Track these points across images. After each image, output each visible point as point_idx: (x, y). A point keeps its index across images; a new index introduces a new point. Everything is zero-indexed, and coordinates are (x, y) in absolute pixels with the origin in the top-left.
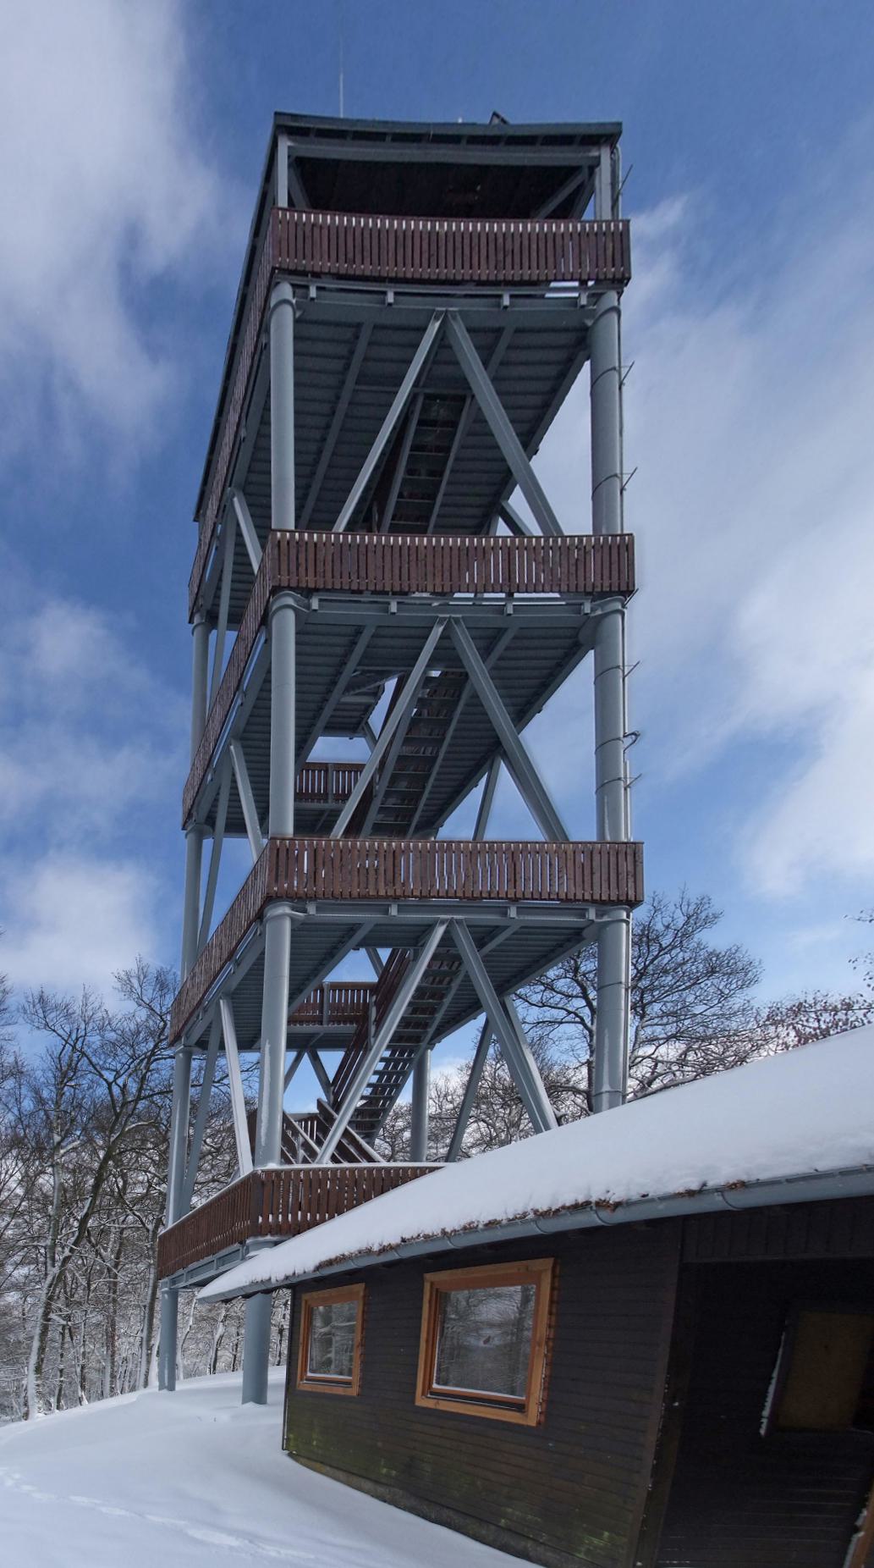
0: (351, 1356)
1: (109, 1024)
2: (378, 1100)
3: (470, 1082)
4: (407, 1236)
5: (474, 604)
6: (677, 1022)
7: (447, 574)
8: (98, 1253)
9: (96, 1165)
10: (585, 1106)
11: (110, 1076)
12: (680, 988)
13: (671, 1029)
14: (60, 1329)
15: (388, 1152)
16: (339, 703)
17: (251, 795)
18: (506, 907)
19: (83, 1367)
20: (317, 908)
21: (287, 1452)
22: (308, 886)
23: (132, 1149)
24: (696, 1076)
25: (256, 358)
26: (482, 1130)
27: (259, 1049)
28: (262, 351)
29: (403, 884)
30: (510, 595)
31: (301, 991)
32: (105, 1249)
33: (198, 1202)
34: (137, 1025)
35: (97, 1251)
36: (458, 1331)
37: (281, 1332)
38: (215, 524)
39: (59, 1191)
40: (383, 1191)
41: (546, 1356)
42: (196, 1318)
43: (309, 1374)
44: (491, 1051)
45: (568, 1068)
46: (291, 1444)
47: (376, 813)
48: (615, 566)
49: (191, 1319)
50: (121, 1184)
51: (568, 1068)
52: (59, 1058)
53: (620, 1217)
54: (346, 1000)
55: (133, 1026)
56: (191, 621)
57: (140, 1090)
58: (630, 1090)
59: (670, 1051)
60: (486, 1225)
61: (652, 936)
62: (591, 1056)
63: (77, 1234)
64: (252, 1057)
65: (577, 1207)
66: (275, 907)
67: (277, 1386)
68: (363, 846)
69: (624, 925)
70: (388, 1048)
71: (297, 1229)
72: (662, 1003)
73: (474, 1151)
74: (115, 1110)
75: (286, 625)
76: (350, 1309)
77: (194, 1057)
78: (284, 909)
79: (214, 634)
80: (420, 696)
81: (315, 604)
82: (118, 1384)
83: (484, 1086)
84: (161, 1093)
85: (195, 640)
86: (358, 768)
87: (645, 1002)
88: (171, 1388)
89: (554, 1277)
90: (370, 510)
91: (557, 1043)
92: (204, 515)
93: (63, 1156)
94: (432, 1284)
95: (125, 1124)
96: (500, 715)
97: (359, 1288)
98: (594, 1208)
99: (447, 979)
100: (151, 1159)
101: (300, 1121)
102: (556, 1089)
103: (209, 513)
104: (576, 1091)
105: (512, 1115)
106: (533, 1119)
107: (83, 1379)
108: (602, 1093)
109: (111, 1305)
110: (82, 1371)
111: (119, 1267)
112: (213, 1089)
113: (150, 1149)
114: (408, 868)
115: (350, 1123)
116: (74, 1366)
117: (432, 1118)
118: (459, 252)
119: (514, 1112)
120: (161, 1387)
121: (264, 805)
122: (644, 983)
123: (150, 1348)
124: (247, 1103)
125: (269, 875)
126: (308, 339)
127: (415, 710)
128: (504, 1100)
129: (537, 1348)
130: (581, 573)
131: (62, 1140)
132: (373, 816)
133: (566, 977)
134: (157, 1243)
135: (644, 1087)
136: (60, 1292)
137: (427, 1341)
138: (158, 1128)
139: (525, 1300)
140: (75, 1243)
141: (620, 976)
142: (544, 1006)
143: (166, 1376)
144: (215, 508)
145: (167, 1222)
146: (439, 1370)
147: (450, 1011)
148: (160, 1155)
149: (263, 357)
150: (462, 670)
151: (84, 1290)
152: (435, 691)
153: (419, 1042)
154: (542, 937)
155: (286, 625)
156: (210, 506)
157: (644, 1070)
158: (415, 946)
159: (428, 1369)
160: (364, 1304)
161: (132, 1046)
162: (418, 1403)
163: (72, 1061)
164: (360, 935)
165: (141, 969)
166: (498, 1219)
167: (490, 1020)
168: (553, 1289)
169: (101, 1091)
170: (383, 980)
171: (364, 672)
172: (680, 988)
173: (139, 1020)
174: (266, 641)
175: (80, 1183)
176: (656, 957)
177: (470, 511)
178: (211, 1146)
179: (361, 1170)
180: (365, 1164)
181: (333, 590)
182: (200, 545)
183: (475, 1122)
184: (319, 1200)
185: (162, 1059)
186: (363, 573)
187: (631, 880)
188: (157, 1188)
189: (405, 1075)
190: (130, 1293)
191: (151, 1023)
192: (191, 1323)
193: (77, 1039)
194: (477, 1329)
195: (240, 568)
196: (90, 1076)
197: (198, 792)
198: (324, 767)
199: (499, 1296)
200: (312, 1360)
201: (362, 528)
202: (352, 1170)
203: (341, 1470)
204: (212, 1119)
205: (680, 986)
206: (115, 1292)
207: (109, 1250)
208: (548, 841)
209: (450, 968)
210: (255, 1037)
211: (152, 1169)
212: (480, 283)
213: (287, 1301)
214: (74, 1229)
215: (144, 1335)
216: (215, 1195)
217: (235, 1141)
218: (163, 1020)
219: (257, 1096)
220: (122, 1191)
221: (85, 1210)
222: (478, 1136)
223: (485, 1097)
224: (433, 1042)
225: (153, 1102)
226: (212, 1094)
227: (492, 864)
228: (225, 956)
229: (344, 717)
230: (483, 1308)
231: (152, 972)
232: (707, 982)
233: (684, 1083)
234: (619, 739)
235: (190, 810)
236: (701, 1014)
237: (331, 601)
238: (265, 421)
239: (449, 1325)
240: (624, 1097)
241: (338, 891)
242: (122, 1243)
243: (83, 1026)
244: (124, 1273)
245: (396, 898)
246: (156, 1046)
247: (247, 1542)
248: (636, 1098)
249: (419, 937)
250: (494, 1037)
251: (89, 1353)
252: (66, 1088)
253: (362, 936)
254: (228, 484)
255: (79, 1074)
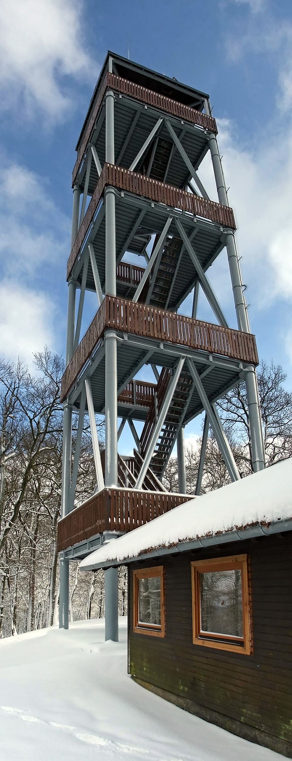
0: (160, 612)
1: (31, 383)
2: (162, 454)
3: (202, 448)
4: (181, 539)
5: (182, 214)
6: (279, 427)
7: (171, 199)
8: (25, 529)
9: (24, 470)
10: (250, 468)
11: (31, 415)
12: (278, 409)
13: (278, 430)
14: (2, 579)
15: (169, 486)
16: (133, 240)
17: (97, 271)
18: (209, 355)
19: (15, 608)
20: (128, 337)
21: (130, 675)
22: (124, 324)
23: (43, 464)
24: (290, 455)
25: (101, 107)
26: (209, 477)
27: (104, 413)
28: (103, 107)
29: (165, 333)
30: (195, 215)
31: (123, 383)
32: (29, 527)
33: (78, 503)
34: (45, 386)
35: (24, 527)
36: (209, 597)
37: (124, 593)
38: (84, 154)
39: (4, 483)
40: (168, 510)
41: (249, 612)
42: (79, 580)
43: (139, 623)
44: (209, 433)
45: (241, 447)
46: (133, 670)
47: (151, 294)
48: (228, 217)
49: (76, 580)
50: (37, 485)
51: (241, 447)
52: (5, 398)
53: (271, 531)
54: (144, 392)
55: (43, 387)
56: (73, 187)
57: (47, 426)
58: (266, 461)
59: (279, 442)
60: (216, 534)
61: (264, 381)
62: (250, 441)
63: (13, 514)
64: (101, 417)
65: (254, 525)
66: (110, 332)
67: (123, 630)
68: (146, 309)
69: (254, 374)
70: (165, 423)
71: (128, 528)
72: (273, 416)
73: (207, 490)
74: (34, 437)
75: (111, 200)
76: (157, 582)
77: (73, 412)
78: (113, 334)
79: (82, 195)
80: (165, 245)
81: (123, 195)
82: (36, 622)
83: (208, 452)
84: (57, 431)
85: (74, 195)
86: (142, 270)
87: (266, 415)
88: (66, 627)
89: (248, 565)
90: (142, 167)
91: (236, 432)
92: (80, 150)
93: (6, 461)
94: (195, 568)
95: (39, 448)
96: (197, 264)
97: (161, 568)
98: (260, 526)
99: (188, 389)
100: (53, 471)
101: (126, 461)
102: (238, 457)
103: (81, 149)
104: (246, 460)
105: (221, 470)
106: (230, 474)
107: (15, 616)
108: (256, 462)
109: (32, 565)
110: (14, 610)
111: (37, 540)
112: (83, 433)
113: (52, 465)
114: (166, 325)
115: (150, 466)
116: (9, 606)
117: (187, 468)
118: (167, 105)
119: (222, 469)
120: (61, 627)
121: (103, 278)
122: (265, 405)
123: (54, 598)
124: (100, 445)
125: (106, 314)
126: (120, 108)
127: (164, 250)
128: (217, 462)
129: (245, 607)
130: (218, 215)
131: (6, 451)
132: (150, 296)
133: (235, 397)
134: (57, 527)
135: (271, 460)
136: (3, 552)
137: (195, 603)
138: (56, 452)
139: (237, 579)
140: (13, 520)
141: (256, 401)
142: (228, 411)
143: (63, 618)
144: (84, 148)
145: (62, 514)
146: (202, 621)
147: (190, 407)
148: (57, 470)
149: (103, 108)
150: (180, 239)
151: (17, 553)
152: (171, 245)
153: (178, 422)
154: (224, 374)
155: (111, 200)
156: (82, 147)
157: (270, 451)
158: (173, 368)
159: (197, 624)
160: (164, 579)
161: (43, 399)
162: (194, 643)
163: (11, 401)
164: (148, 356)
165: (47, 353)
166: (221, 531)
167: (207, 415)
168: (248, 572)
169: (27, 423)
170: (160, 384)
171: (143, 228)
172: (278, 409)
173: (46, 384)
174: (103, 204)
175: (15, 480)
176: (267, 392)
177: (178, 180)
178: (83, 469)
179: (157, 495)
180: (158, 492)
181: (129, 191)
182: (77, 160)
183: (206, 472)
184: (138, 512)
185: (57, 409)
186: (140, 189)
187: (253, 352)
188: (57, 491)
189: (172, 440)
190: (43, 558)
191: (52, 387)
192: (76, 583)
193: (15, 389)
194: (218, 596)
195: (93, 173)
196: (21, 413)
197: (74, 264)
198: (128, 266)
199: (225, 576)
200: (140, 613)
201: (140, 173)
202: (153, 495)
203: (159, 688)
204: (83, 452)
205: (278, 408)
206: (34, 557)
207: (31, 528)
208: (221, 326)
209: (188, 383)
210: (102, 406)
211: (53, 478)
212: (173, 115)
213: (126, 573)
214: (12, 511)
215: (51, 588)
216: (86, 501)
217: (95, 468)
218: (57, 386)
219: (105, 442)
220: (38, 490)
221: (18, 499)
222: (208, 481)
223: (209, 459)
224: (184, 423)
225: (53, 436)
226: (83, 436)
227: (200, 331)
228: (87, 355)
229: (136, 245)
230: (219, 583)
231: (52, 356)
232: (286, 408)
233: (286, 459)
234: (240, 286)
235: (70, 272)
236: (287, 423)
237: (130, 196)
238: (104, 126)
239: (204, 594)
240: (265, 464)
241: (137, 330)
242: (38, 523)
243: (17, 381)
244: (39, 545)
245: (162, 340)
246: (54, 401)
247: (110, 742)
248: (270, 466)
249: (174, 363)
250: (210, 425)
251: (19, 598)
252: (8, 418)
253: (149, 357)
254: (89, 142)
255: (15, 410)
